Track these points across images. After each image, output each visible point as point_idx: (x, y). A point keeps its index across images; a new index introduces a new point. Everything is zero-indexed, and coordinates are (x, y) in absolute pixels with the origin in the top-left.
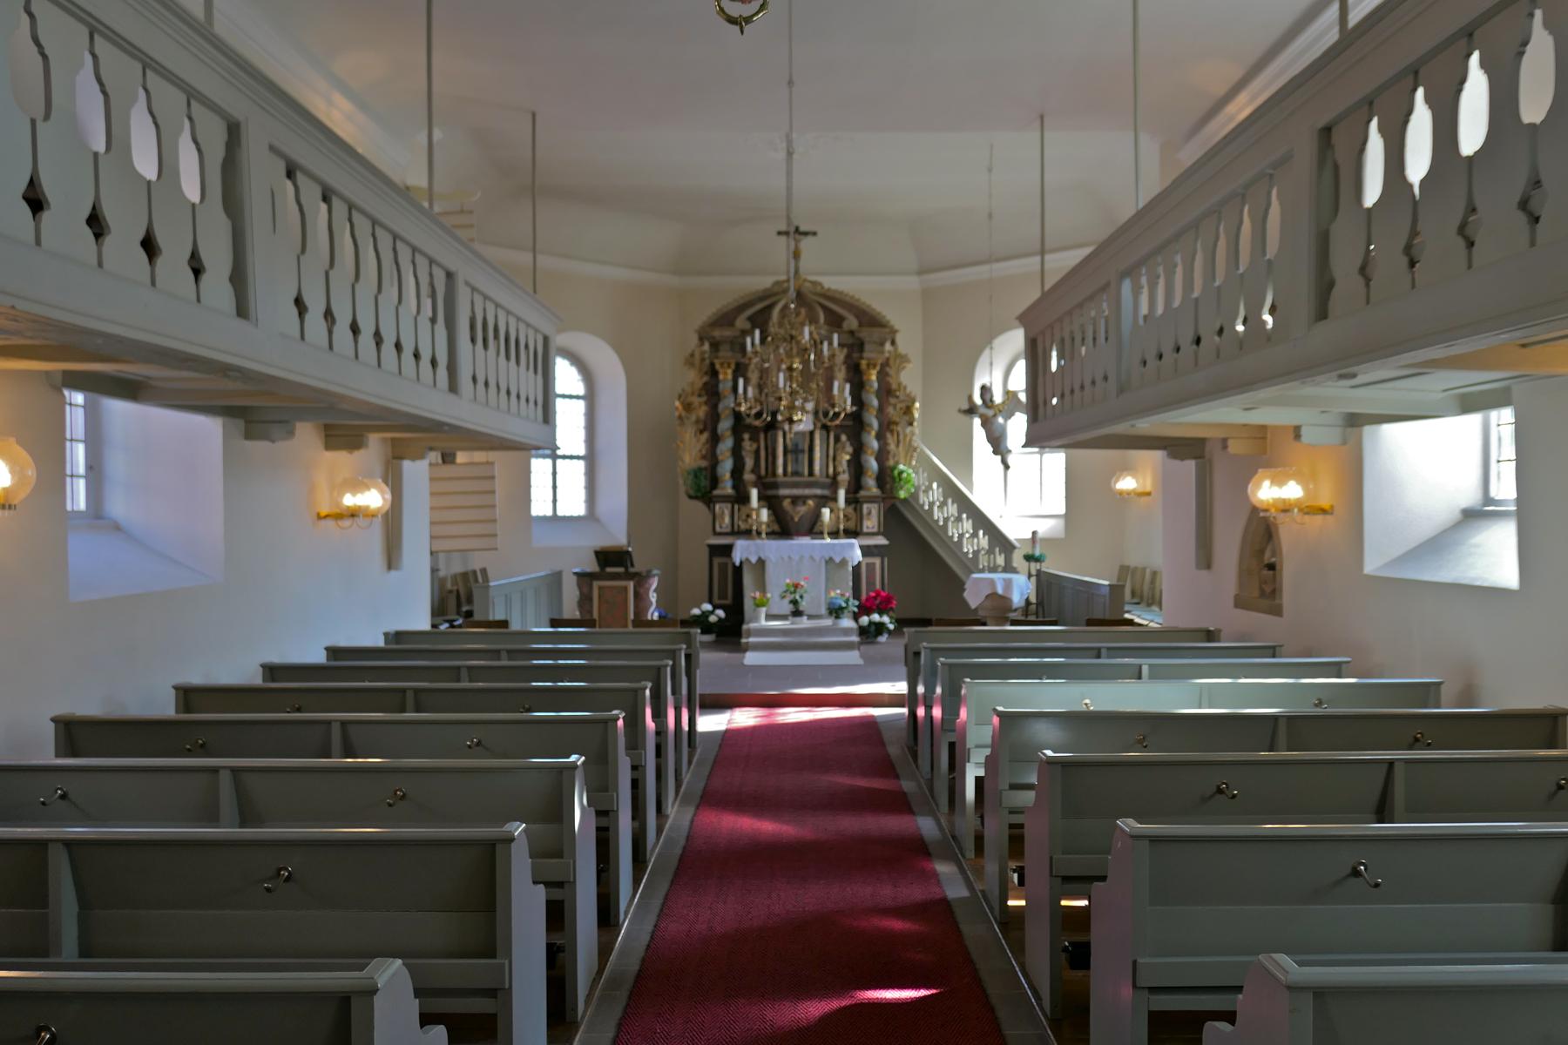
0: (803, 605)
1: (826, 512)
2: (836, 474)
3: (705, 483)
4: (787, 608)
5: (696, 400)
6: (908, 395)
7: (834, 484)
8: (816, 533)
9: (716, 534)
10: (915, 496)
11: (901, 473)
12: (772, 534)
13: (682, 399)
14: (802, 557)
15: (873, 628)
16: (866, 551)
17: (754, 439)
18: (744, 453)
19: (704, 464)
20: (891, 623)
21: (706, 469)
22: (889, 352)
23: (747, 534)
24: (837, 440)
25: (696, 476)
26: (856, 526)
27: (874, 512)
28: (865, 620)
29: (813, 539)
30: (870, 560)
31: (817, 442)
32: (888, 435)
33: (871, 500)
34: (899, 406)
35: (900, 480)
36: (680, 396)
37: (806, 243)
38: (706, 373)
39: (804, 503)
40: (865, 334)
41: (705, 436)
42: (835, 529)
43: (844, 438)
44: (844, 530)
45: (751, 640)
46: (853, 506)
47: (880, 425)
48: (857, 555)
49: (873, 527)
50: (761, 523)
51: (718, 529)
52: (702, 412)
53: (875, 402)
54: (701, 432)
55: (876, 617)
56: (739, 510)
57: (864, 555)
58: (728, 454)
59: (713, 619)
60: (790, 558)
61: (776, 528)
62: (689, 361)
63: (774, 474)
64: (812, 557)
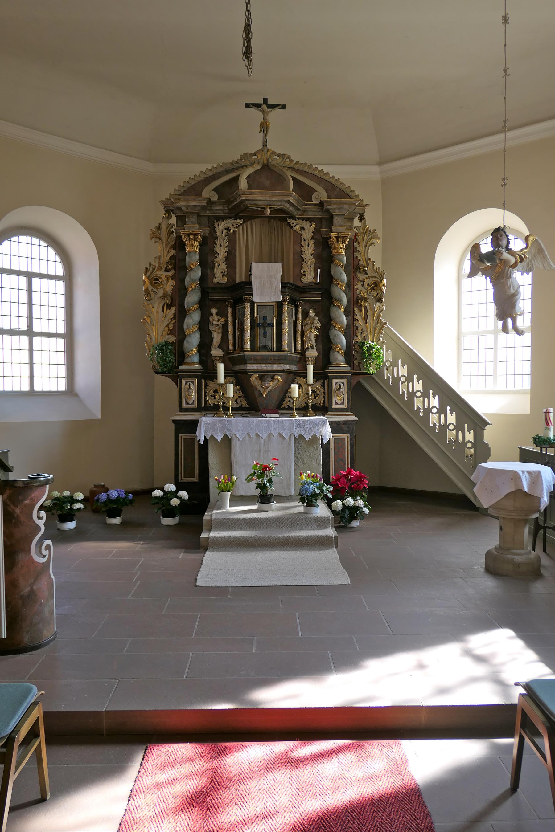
0: (272, 490)
1: (295, 387)
2: (304, 350)
3: (170, 358)
4: (252, 489)
5: (163, 274)
6: (376, 271)
7: (303, 360)
8: (284, 409)
9: (182, 409)
10: (380, 373)
11: (370, 348)
12: (239, 411)
13: (148, 274)
14: (270, 435)
15: (347, 512)
16: (336, 427)
17: (222, 314)
18: (211, 328)
19: (171, 339)
20: (366, 506)
21: (173, 344)
22: (357, 228)
23: (213, 410)
24: (306, 315)
25: (161, 350)
26: (324, 401)
27: (344, 388)
28: (338, 504)
29: (281, 415)
30: (340, 437)
31: (286, 315)
32: (357, 311)
33: (341, 375)
34: (367, 282)
35: (370, 355)
36: (147, 270)
37: (274, 115)
38: (173, 247)
39: (273, 378)
40: (334, 206)
41: (173, 310)
42: (303, 405)
43: (312, 313)
44: (312, 405)
45: (214, 534)
46: (321, 381)
47: (348, 301)
48: (327, 433)
49: (342, 404)
50: (228, 399)
51: (184, 405)
52: (169, 286)
53: (345, 277)
54: (169, 306)
55: (350, 501)
56: (206, 385)
57: (334, 431)
58: (195, 328)
59: (175, 502)
60: (257, 435)
61: (244, 403)
62: (156, 235)
63: (242, 349)
64: (280, 435)
